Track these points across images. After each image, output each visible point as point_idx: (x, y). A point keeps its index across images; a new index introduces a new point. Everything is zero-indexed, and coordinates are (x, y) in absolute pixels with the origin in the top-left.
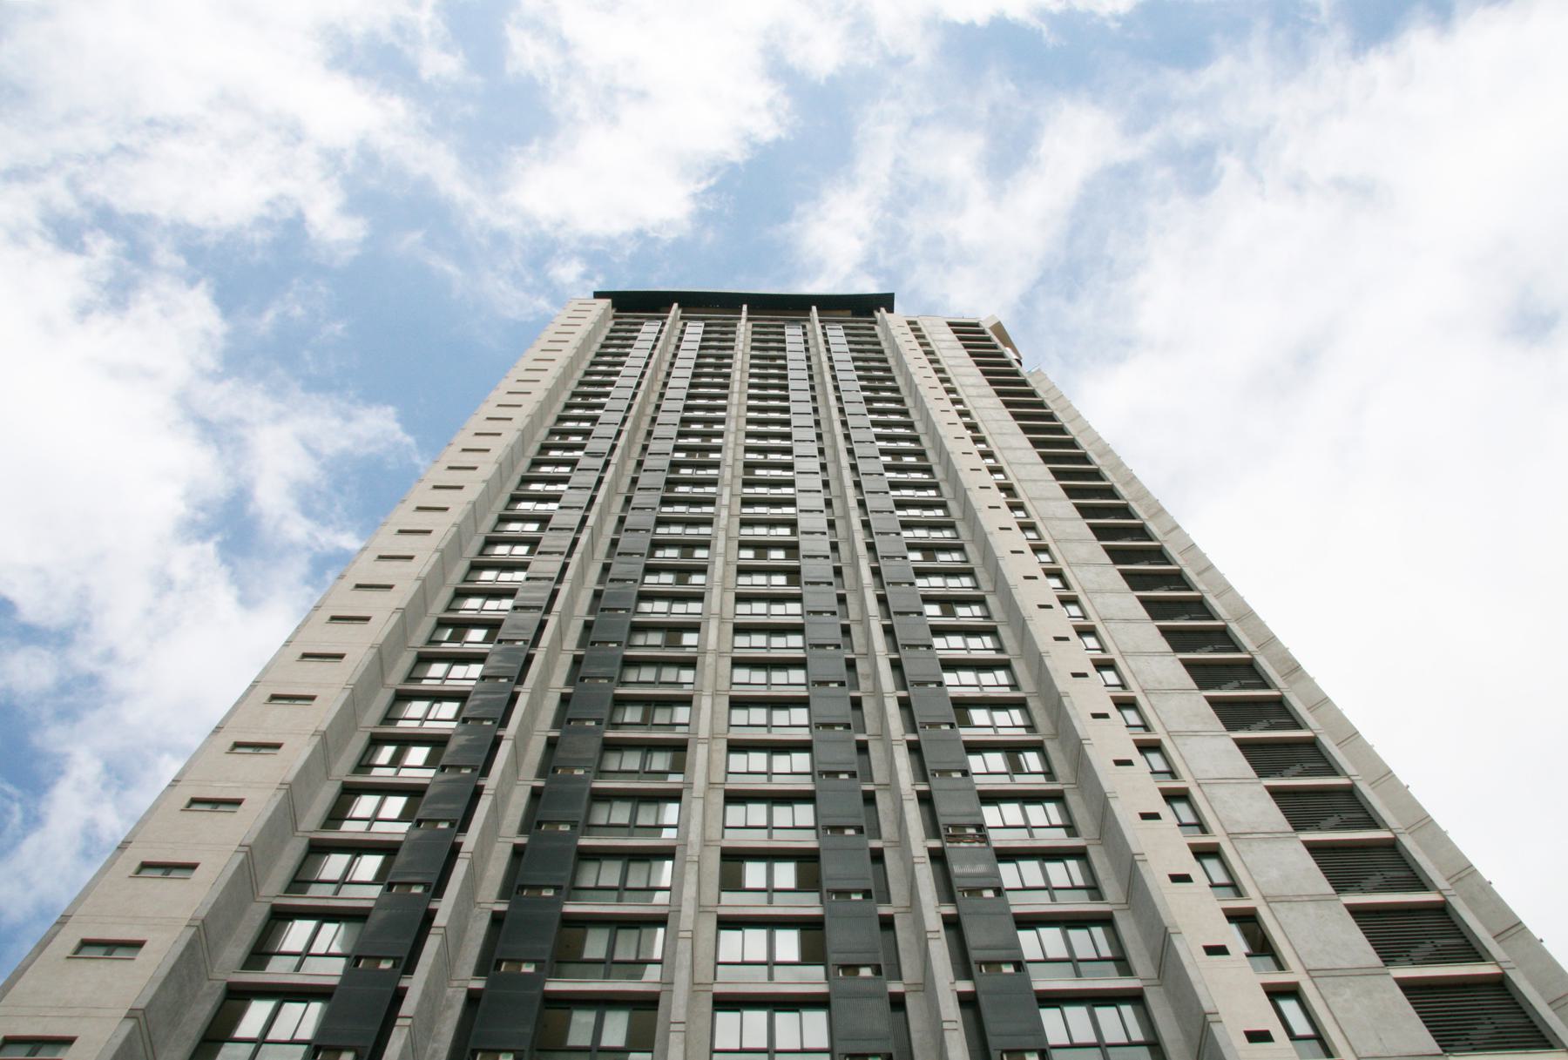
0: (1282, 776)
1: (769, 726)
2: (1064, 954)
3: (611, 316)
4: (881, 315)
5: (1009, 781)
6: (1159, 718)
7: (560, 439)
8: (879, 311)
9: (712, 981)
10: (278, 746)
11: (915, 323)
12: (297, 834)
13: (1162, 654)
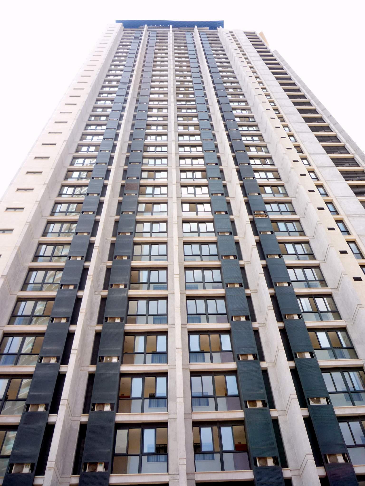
0: (364, 196)
1: (190, 140)
2: (304, 279)
3: (122, 30)
4: (220, 29)
5: (267, 180)
6: (323, 176)
7: (108, 83)
8: (219, 27)
9: (190, 412)
10: (33, 189)
11: (232, 32)
12: (43, 217)
13: (323, 154)
